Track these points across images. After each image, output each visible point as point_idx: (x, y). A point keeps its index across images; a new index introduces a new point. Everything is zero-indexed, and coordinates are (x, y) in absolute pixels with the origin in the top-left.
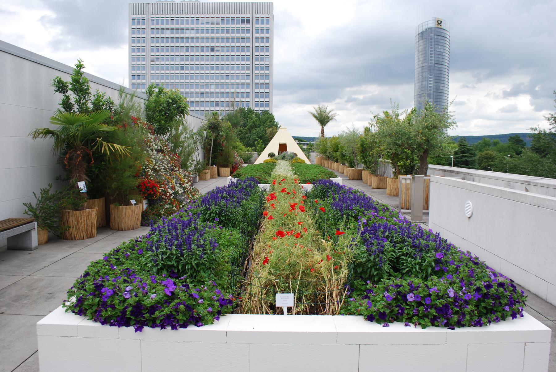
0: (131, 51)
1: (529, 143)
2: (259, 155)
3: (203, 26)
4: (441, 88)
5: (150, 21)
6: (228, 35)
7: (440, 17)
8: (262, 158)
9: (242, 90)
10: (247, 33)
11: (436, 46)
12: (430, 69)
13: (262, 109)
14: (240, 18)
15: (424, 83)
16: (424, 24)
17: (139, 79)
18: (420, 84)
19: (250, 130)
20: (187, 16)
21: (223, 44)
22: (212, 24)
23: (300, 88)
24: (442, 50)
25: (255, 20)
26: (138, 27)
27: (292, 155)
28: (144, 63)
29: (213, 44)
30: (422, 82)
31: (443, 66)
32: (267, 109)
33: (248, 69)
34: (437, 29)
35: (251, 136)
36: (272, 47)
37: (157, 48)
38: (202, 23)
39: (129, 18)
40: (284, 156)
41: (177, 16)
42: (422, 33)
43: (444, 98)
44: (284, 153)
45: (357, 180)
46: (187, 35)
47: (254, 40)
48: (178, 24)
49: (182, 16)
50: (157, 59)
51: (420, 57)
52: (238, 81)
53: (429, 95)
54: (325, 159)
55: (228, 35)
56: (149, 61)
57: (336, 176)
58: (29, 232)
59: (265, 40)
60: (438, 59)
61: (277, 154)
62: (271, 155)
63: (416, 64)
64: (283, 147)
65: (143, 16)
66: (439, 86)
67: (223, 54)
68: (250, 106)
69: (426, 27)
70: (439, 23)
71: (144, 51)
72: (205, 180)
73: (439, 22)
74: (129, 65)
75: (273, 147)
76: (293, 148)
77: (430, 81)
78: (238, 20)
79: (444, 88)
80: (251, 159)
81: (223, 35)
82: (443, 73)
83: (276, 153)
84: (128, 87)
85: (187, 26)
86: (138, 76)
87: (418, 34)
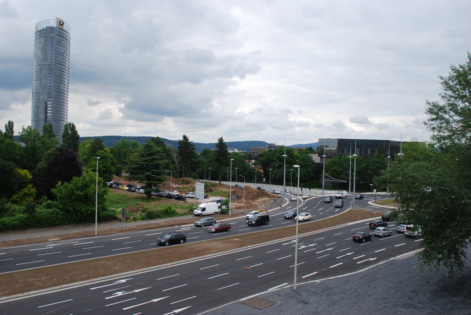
1: (141, 147)
4: (62, 88)
12: (50, 69)
16: (45, 22)
24: (63, 51)
53: (50, 95)
66: (60, 86)
69: (48, 26)
73: (61, 23)
82: (63, 73)
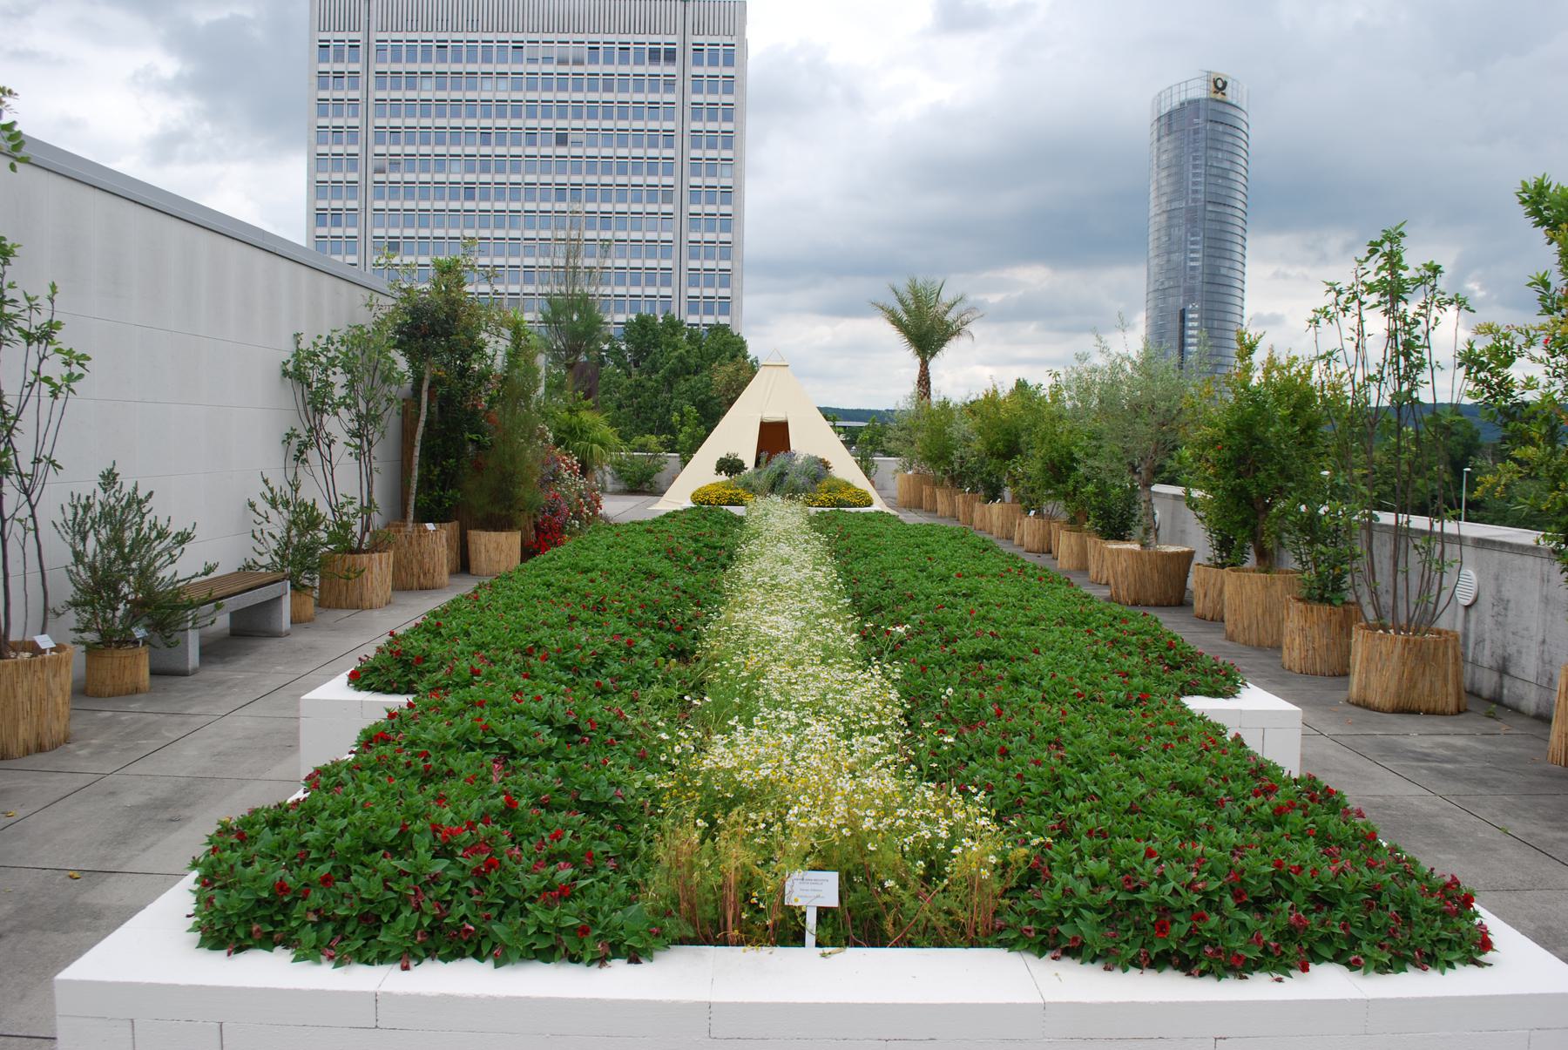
2: (686, 463)
3: (533, 68)
4: (1224, 271)
6: (608, 97)
7: (1222, 70)
8: (695, 477)
9: (650, 263)
13: (709, 320)
14: (647, 46)
15: (1175, 257)
16: (1175, 90)
17: (337, 224)
18: (1163, 260)
19: (669, 382)
20: (488, 37)
21: (592, 124)
23: (820, 272)
24: (1227, 165)
26: (339, 67)
27: (814, 468)
28: (353, 177)
29: (562, 124)
30: (1169, 253)
31: (1229, 210)
32: (723, 320)
33: (667, 198)
34: (1212, 105)
35: (671, 399)
36: (743, 132)
37: (395, 131)
38: (533, 60)
40: (782, 475)
41: (457, 36)
42: (1170, 114)
43: (1232, 300)
44: (779, 460)
45: (1169, 605)
46: (485, 96)
47: (688, 112)
48: (458, 60)
49: (472, 37)
50: (395, 165)
51: (1164, 182)
52: (636, 235)
54: (937, 483)
55: (608, 97)
56: (370, 170)
57: (1223, 684)
58: (279, 598)
59: (720, 113)
60: (1214, 189)
61: (750, 463)
62: (729, 466)
63: (1152, 205)
64: (774, 436)
65: (354, 36)
66: (1219, 267)
67: (592, 152)
68: (674, 310)
69: (1183, 98)
70: (1220, 86)
71: (354, 141)
72: (358, 605)
73: (1220, 85)
74: (309, 182)
75: (736, 435)
76: (813, 440)
77: (1193, 251)
78: (639, 53)
79: (1232, 273)
80: (656, 477)
81: (593, 96)
82: (1230, 228)
83: (749, 458)
84: (303, 243)
85: (487, 68)
86: (337, 216)
87: (1159, 119)
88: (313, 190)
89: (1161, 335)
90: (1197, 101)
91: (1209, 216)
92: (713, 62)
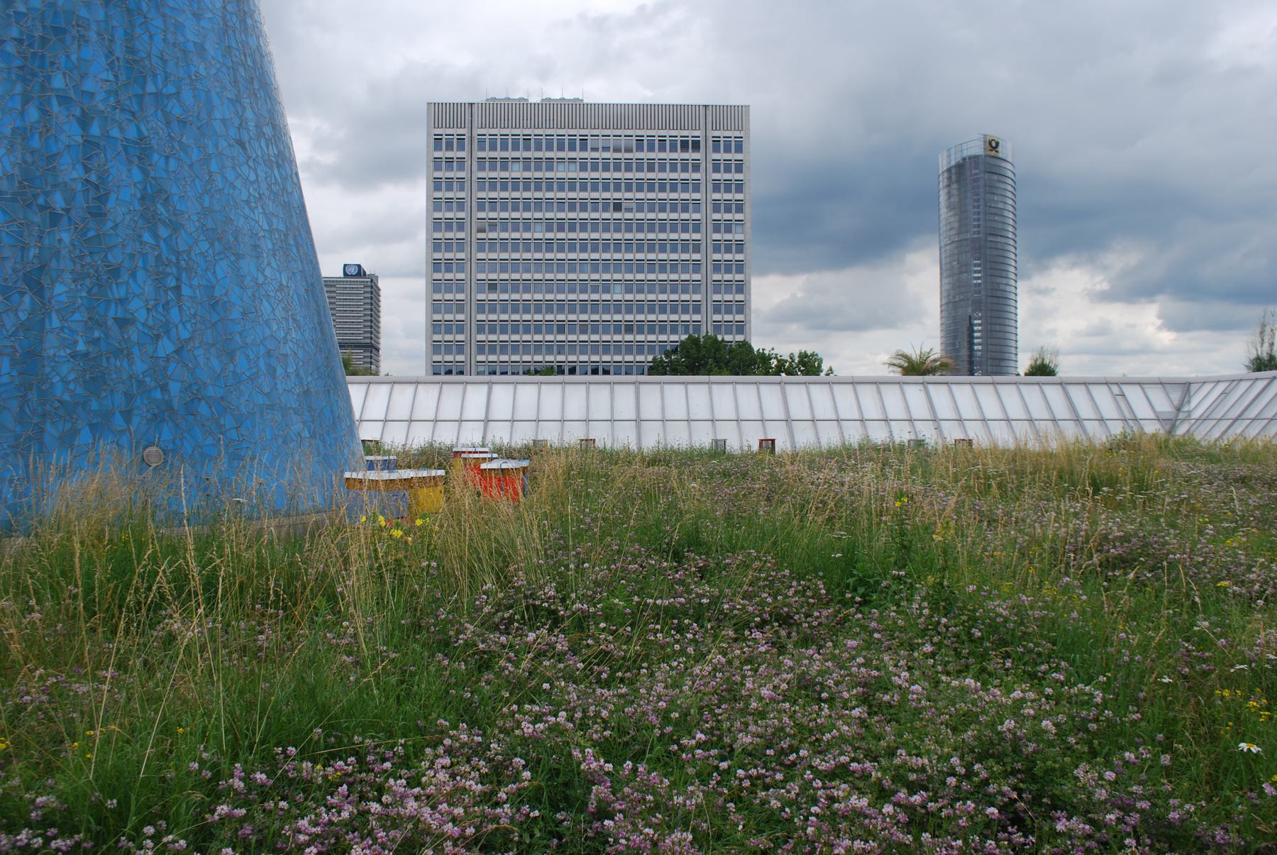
0: (431, 208)
5: (475, 142)
7: (994, 133)
10: (694, 171)
11: (989, 196)
14: (679, 139)
22: (617, 150)
25: (710, 143)
31: (1003, 240)
37: (493, 202)
38: (595, 149)
39: (428, 135)
46: (560, 175)
50: (493, 227)
56: (474, 231)
65: (461, 131)
70: (993, 145)
88: (431, 245)
89: (955, 338)
90: (976, 157)
91: (989, 244)
92: (727, 150)
